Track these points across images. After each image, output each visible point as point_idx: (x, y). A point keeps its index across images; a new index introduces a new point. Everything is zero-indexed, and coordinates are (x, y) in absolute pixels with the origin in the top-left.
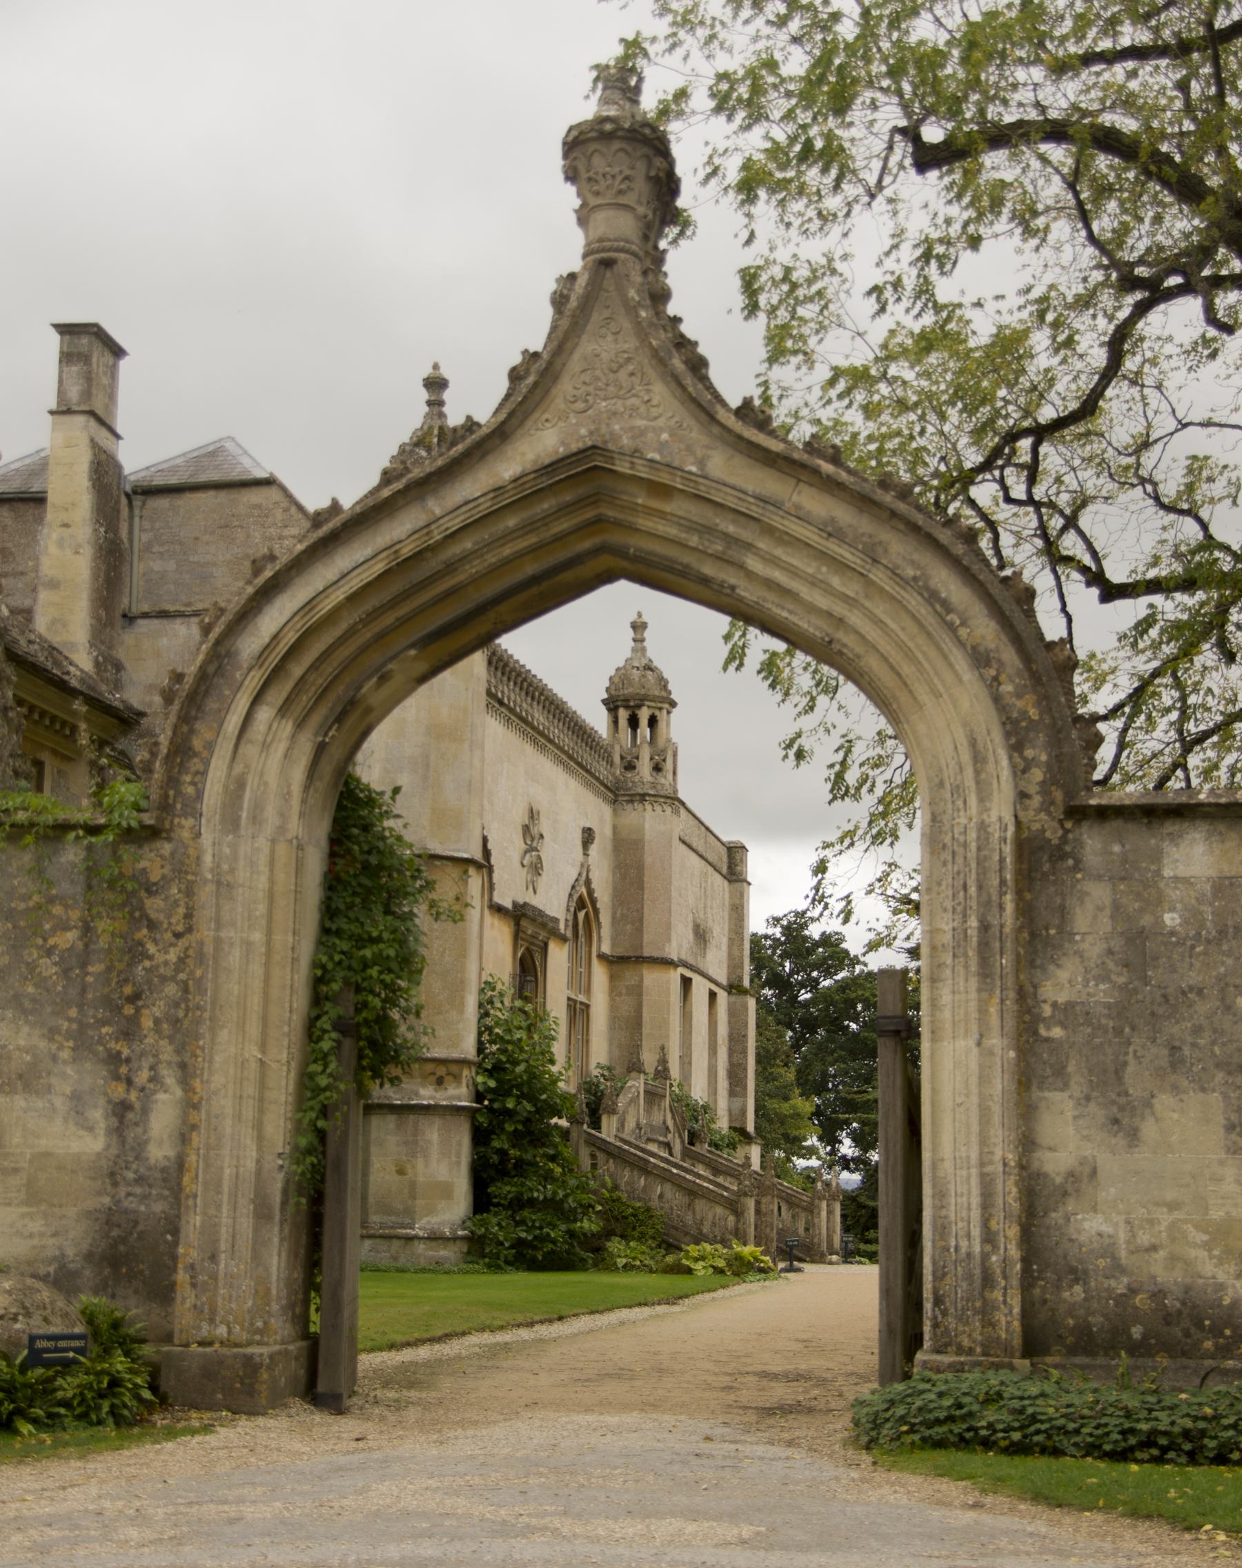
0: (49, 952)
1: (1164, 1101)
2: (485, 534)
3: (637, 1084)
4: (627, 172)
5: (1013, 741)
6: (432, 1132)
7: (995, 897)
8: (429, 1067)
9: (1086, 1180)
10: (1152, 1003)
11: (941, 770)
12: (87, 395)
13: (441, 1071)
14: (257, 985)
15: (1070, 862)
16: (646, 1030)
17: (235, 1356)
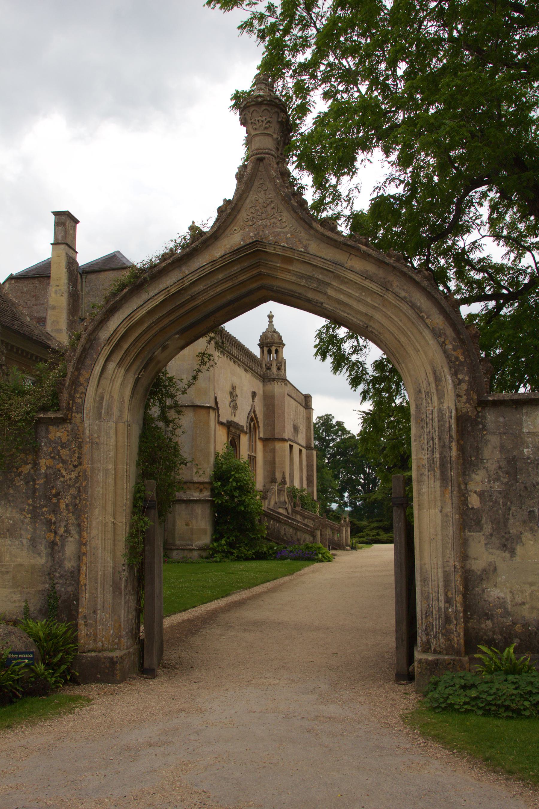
0: (19, 474)
6: (199, 510)
7: (447, 443)
8: (197, 485)
9: (491, 573)
10: (520, 490)
12: (65, 237)
13: (201, 487)
14: (111, 488)
15: (481, 426)
16: (277, 465)
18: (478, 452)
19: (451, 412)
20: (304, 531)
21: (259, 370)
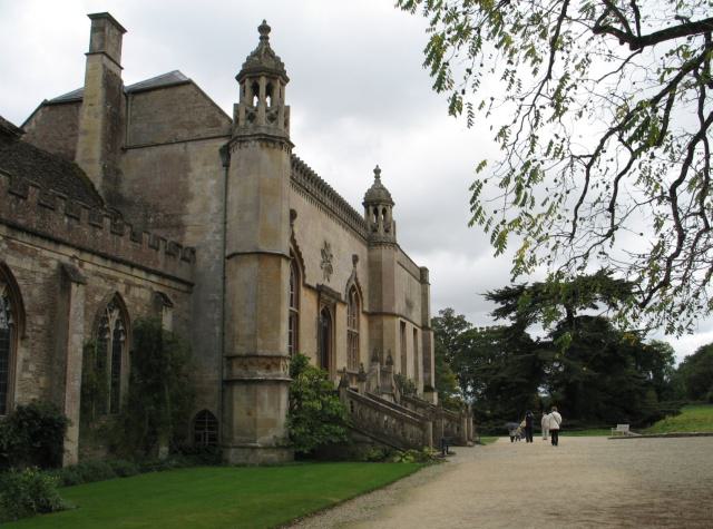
12: (102, 45)
13: (269, 362)
20: (411, 422)
21: (363, 232)
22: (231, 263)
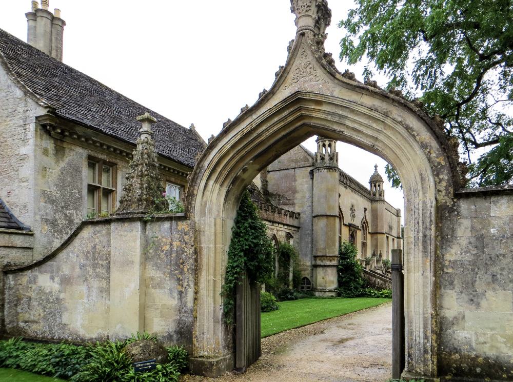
0: (163, 252)
1: (490, 294)
2: (268, 124)
3: (375, 258)
4: (308, 4)
5: (435, 173)
6: (329, 270)
7: (428, 226)
9: (461, 319)
10: (486, 260)
11: (410, 185)
13: (331, 258)
14: (212, 259)
15: (456, 213)
17: (207, 362)
18: (453, 231)
19: (432, 203)
21: (369, 196)
22: (316, 219)
